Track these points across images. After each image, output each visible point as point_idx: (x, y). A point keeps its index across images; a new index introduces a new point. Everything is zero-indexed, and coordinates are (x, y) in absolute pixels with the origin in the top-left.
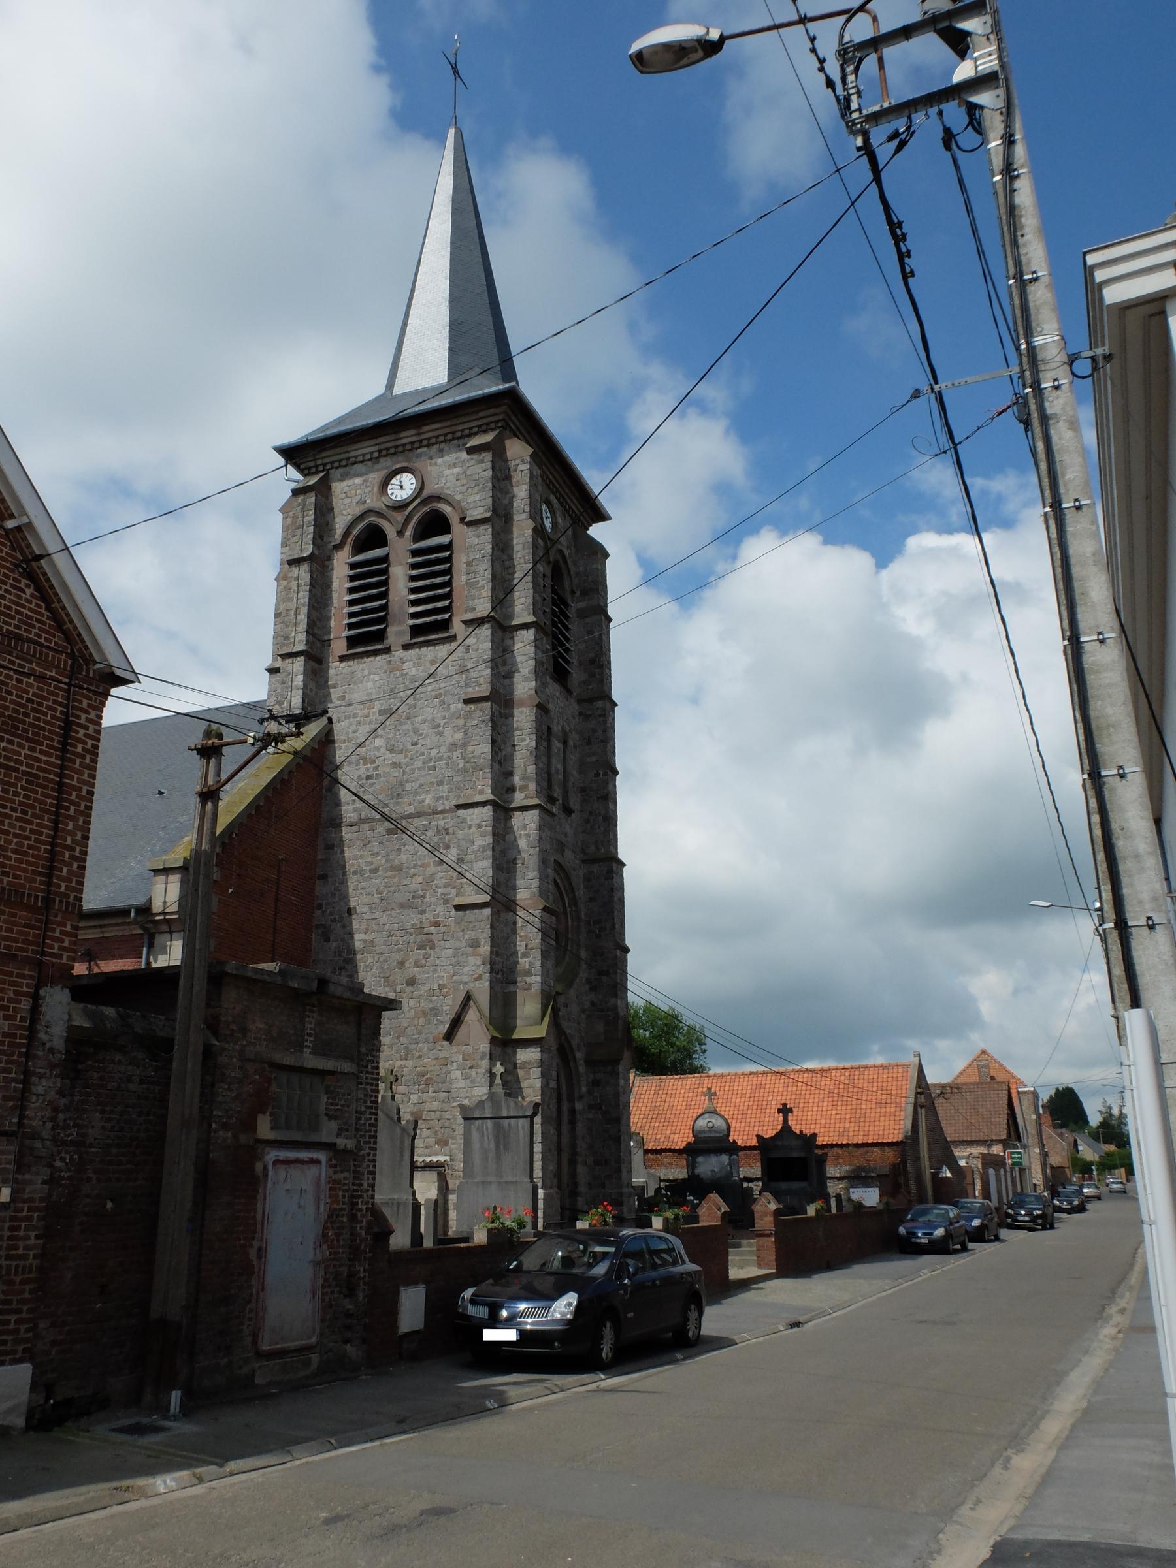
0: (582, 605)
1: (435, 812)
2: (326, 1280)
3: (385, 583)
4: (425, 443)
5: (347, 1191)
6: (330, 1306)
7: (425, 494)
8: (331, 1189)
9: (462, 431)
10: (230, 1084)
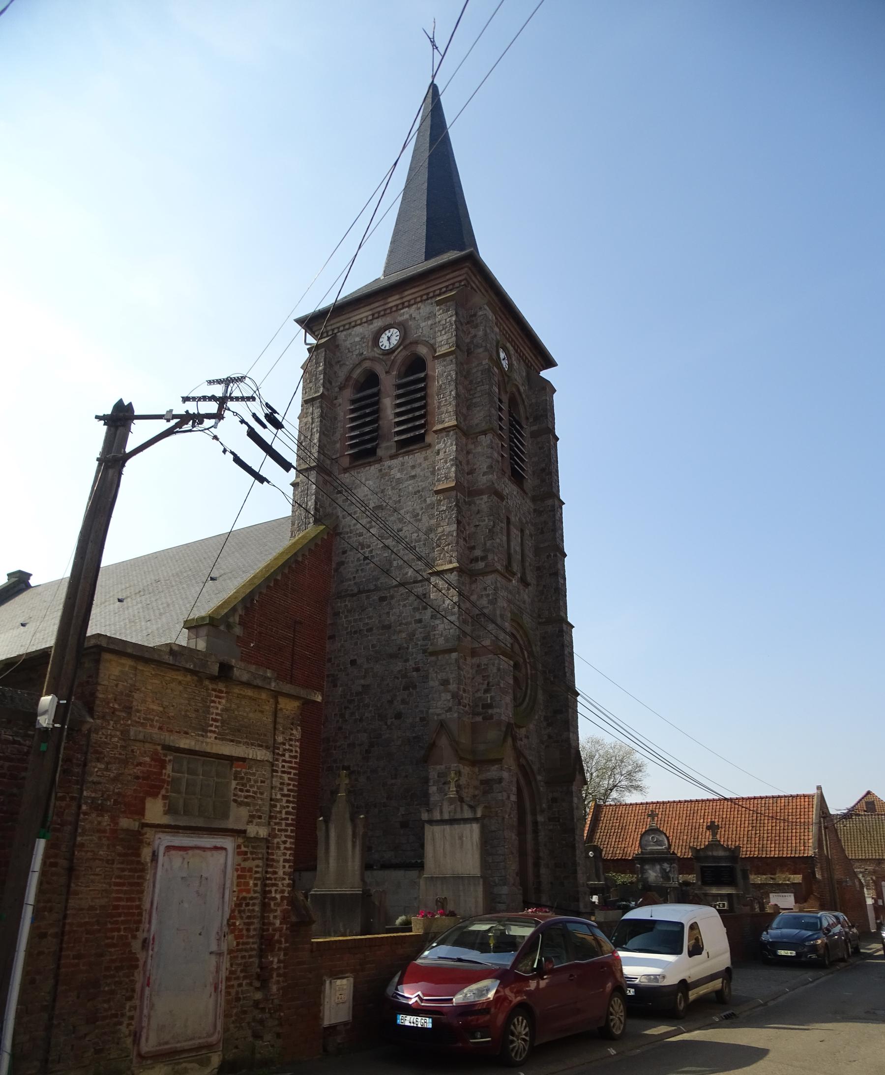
0: (535, 428)
1: (415, 582)
2: (231, 972)
3: (377, 411)
4: (406, 304)
5: (258, 879)
6: (238, 999)
7: (408, 342)
8: (239, 877)
9: (434, 291)
10: (108, 764)
